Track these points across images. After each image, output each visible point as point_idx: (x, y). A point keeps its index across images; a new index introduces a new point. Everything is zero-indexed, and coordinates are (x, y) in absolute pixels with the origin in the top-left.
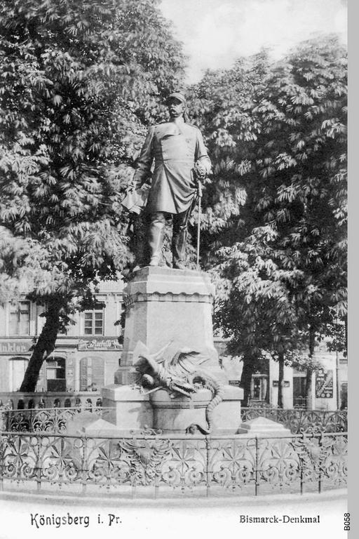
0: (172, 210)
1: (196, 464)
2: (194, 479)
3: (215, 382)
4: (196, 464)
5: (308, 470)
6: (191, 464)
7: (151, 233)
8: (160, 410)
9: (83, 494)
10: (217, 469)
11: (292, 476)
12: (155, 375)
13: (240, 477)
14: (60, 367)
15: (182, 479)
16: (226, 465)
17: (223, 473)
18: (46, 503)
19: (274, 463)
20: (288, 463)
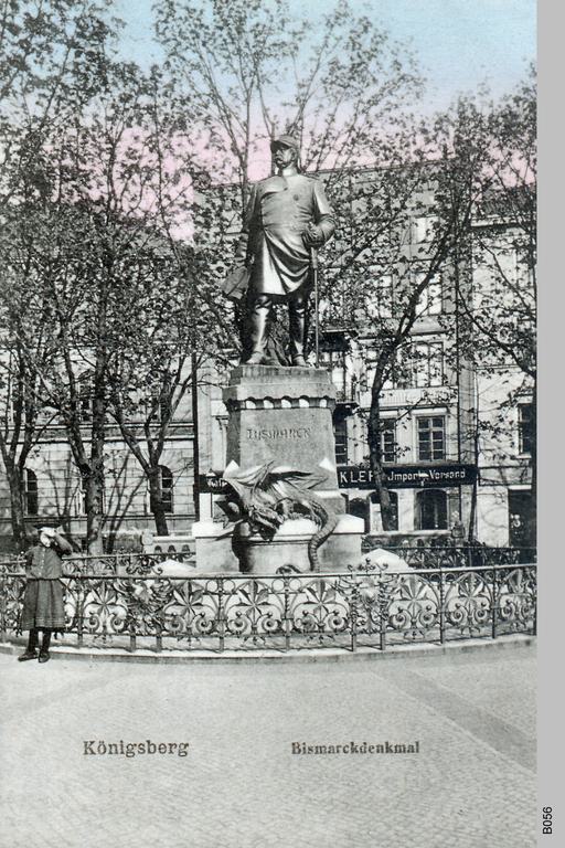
0: (279, 290)
1: (204, 610)
2: (203, 629)
3: (324, 511)
4: (204, 610)
5: (360, 619)
6: (265, 610)
7: (253, 322)
8: (257, 547)
9: (159, 648)
10: (452, 608)
11: (428, 622)
12: (240, 503)
13: (197, 626)
14: (393, 490)
15: (254, 629)
16: (462, 602)
17: (239, 621)
18: (76, 659)
19: (404, 605)
20: (424, 607)
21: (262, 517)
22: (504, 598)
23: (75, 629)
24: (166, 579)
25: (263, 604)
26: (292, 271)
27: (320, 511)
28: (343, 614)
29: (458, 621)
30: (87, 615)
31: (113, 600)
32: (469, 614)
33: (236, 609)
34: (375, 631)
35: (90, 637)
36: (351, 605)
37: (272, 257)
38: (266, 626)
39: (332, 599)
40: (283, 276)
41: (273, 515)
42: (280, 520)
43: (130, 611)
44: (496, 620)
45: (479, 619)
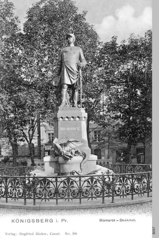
2: (19, 195)
6: (72, 189)
21: (66, 155)
22: (118, 186)
23: (5, 196)
24: (37, 178)
25: (95, 186)
26: (74, 77)
27: (84, 153)
28: (100, 190)
29: (87, 195)
30: (9, 191)
31: (18, 186)
32: (141, 189)
33: (86, 188)
34: (110, 196)
35: (10, 199)
36: (102, 187)
37: (66, 69)
38: (73, 196)
39: (72, 186)
40: (70, 78)
41: (70, 154)
42: (72, 156)
43: (24, 190)
44: (141, 192)
45: (127, 192)
